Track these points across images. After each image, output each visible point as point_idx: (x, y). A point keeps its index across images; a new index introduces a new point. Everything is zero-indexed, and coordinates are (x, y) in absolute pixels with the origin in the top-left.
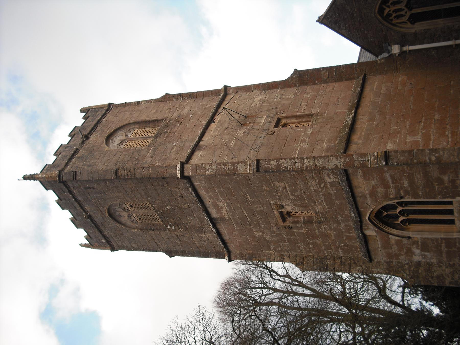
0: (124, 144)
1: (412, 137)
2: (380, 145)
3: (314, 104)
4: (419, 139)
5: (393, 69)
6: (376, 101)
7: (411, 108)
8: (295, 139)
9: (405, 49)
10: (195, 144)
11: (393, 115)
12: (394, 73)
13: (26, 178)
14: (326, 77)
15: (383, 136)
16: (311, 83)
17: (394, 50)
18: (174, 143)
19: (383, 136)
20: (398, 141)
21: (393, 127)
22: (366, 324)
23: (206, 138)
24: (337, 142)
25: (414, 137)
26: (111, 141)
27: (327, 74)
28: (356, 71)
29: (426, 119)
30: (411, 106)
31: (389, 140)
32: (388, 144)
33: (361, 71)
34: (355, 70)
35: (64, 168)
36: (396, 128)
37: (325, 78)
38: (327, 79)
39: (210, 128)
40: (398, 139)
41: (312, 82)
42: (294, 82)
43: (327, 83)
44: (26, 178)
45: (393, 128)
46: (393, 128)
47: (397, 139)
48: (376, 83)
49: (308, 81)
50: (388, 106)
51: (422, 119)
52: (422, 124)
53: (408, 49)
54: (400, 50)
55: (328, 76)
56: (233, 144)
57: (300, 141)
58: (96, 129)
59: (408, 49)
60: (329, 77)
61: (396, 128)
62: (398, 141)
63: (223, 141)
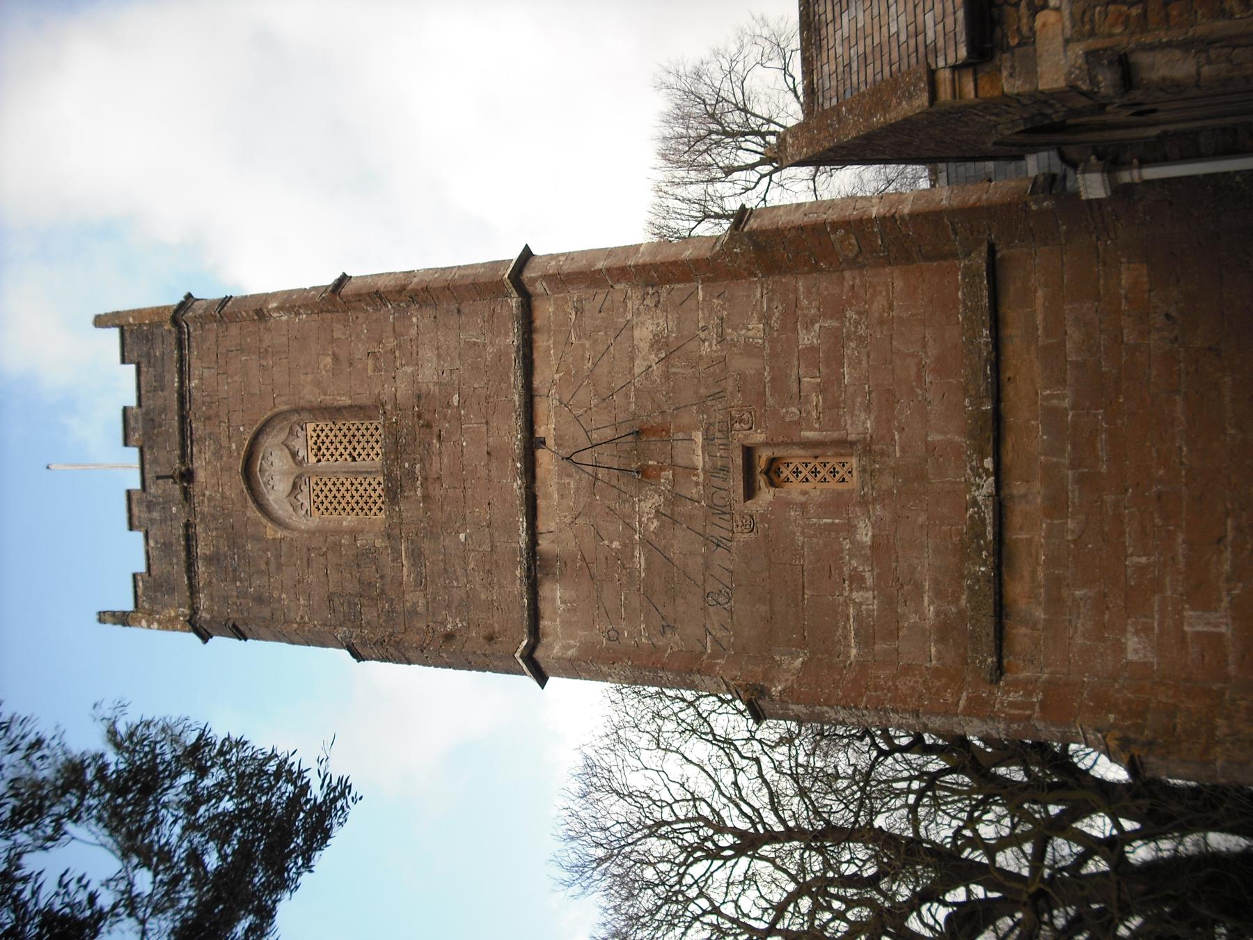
0: (305, 489)
1: (1199, 613)
2: (1104, 639)
3: (846, 386)
4: (1223, 629)
5: (1091, 228)
6: (1055, 402)
7: (1182, 463)
8: (827, 568)
9: (1126, 177)
10: (528, 554)
11: (1127, 490)
12: (1098, 239)
13: (103, 617)
14: (851, 250)
15: (1105, 595)
16: (806, 269)
17: (1086, 189)
18: (458, 533)
19: (1105, 595)
20: (1156, 625)
21: (1132, 555)
22: (1123, 858)
23: (543, 524)
24: (963, 602)
25: (1207, 615)
26: (262, 477)
27: (853, 241)
28: (956, 234)
29: (1238, 529)
30: (1180, 448)
31: (1128, 617)
32: (1129, 636)
33: (975, 233)
34: (951, 232)
35: (193, 603)
36: (1143, 560)
37: (851, 255)
38: (857, 256)
39: (540, 472)
40: (1157, 616)
41: (805, 265)
42: (744, 266)
43: (862, 267)
44: (103, 617)
45: (1136, 559)
46: (1136, 559)
47: (1153, 618)
48: (1040, 293)
49: (790, 261)
50: (1103, 436)
51: (1225, 524)
52: (1228, 555)
53: (1140, 177)
54: (1109, 190)
55: (857, 248)
56: (643, 566)
57: (846, 577)
58: (191, 433)
59: (1140, 177)
60: (864, 250)
61: (1143, 560)
62: (1156, 625)
63: (606, 542)
